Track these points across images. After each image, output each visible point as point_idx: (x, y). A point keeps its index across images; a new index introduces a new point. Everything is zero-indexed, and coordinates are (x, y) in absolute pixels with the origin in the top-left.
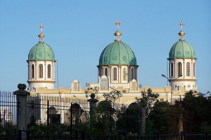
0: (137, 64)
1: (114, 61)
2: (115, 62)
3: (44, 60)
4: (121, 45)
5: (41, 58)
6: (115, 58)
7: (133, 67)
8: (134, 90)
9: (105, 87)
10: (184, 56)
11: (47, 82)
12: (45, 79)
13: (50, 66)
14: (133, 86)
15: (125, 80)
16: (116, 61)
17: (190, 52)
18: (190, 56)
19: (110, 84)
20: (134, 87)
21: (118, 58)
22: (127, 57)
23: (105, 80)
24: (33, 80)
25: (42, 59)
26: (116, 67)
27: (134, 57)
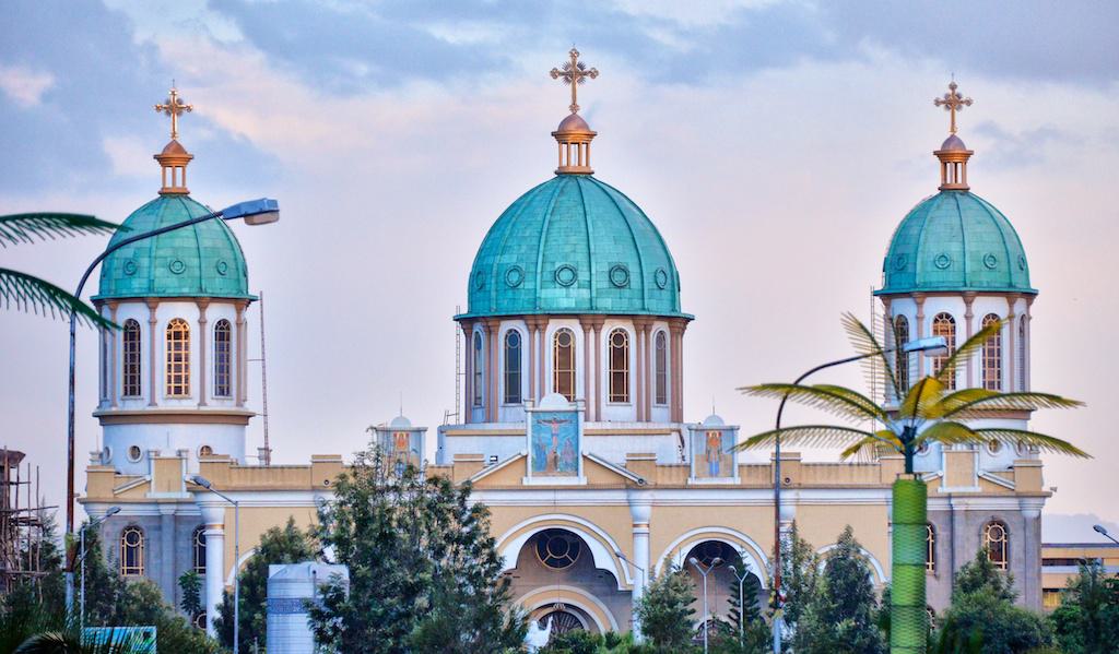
0: (685, 310)
1: (560, 292)
2: (567, 296)
3: (193, 299)
4: (597, 206)
5: (180, 287)
6: (566, 276)
7: (663, 326)
8: (716, 476)
9: (559, 454)
10: (968, 282)
11: (212, 419)
12: (202, 403)
13: (228, 328)
14: (708, 452)
15: (621, 399)
16: (573, 291)
17: (1001, 257)
18: (999, 281)
19: (520, 427)
20: (713, 455)
21: (583, 276)
22: (633, 269)
23: (560, 417)
24: (133, 406)
25: (186, 291)
26: (574, 326)
27: (914, 565)
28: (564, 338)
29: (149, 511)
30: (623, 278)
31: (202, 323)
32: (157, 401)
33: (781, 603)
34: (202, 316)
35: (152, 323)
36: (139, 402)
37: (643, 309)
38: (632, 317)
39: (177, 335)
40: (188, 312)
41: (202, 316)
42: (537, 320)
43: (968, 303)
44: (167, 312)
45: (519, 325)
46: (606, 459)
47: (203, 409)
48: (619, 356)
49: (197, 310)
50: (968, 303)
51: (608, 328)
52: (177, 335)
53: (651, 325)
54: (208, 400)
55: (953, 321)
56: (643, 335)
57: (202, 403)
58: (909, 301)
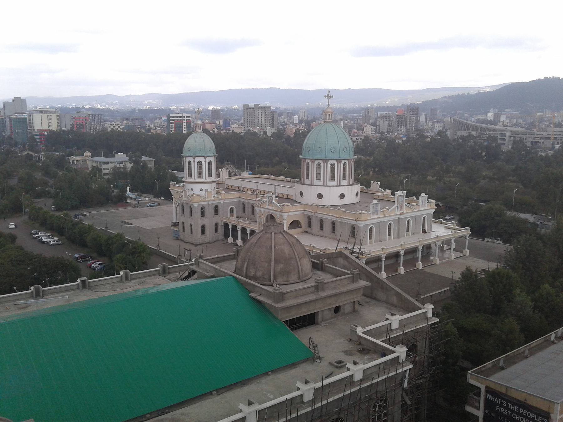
12: (206, 179)
15: (333, 180)
28: (333, 165)
29: (206, 203)
30: (334, 150)
31: (205, 162)
32: (196, 179)
33: (52, 191)
34: (205, 160)
35: (194, 161)
36: (191, 179)
37: (339, 157)
38: (336, 160)
39: (200, 164)
40: (202, 159)
41: (194, 160)
42: (313, 160)
43: (205, 159)
44: (197, 159)
45: (321, 162)
46: (291, 188)
47: (206, 181)
48: (332, 170)
49: (204, 159)
50: (205, 159)
51: (330, 163)
52: (200, 164)
53: (341, 162)
54: (207, 179)
55: (202, 162)
56: (339, 164)
57: (195, 180)
58: (192, 158)
